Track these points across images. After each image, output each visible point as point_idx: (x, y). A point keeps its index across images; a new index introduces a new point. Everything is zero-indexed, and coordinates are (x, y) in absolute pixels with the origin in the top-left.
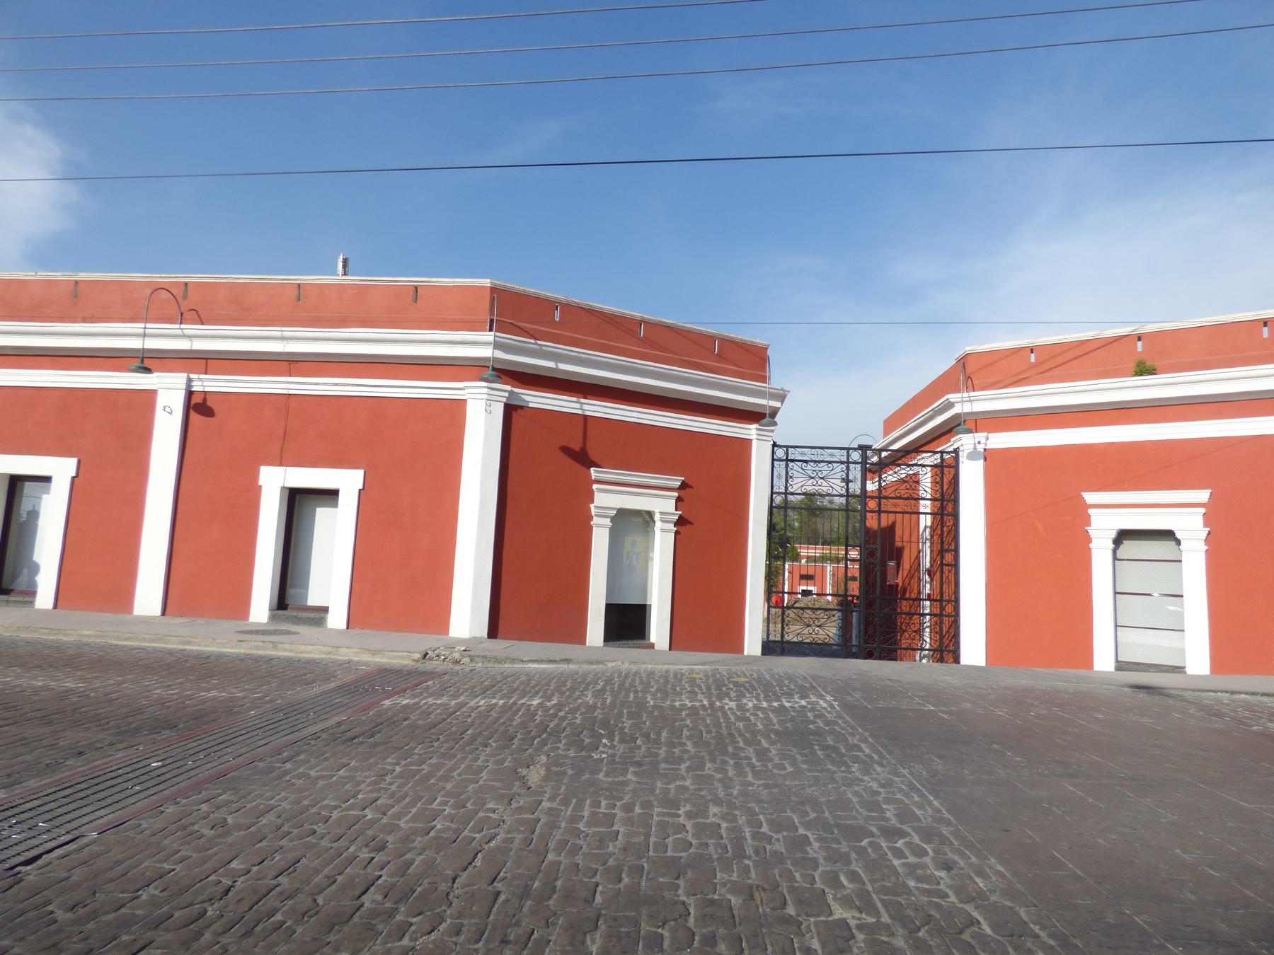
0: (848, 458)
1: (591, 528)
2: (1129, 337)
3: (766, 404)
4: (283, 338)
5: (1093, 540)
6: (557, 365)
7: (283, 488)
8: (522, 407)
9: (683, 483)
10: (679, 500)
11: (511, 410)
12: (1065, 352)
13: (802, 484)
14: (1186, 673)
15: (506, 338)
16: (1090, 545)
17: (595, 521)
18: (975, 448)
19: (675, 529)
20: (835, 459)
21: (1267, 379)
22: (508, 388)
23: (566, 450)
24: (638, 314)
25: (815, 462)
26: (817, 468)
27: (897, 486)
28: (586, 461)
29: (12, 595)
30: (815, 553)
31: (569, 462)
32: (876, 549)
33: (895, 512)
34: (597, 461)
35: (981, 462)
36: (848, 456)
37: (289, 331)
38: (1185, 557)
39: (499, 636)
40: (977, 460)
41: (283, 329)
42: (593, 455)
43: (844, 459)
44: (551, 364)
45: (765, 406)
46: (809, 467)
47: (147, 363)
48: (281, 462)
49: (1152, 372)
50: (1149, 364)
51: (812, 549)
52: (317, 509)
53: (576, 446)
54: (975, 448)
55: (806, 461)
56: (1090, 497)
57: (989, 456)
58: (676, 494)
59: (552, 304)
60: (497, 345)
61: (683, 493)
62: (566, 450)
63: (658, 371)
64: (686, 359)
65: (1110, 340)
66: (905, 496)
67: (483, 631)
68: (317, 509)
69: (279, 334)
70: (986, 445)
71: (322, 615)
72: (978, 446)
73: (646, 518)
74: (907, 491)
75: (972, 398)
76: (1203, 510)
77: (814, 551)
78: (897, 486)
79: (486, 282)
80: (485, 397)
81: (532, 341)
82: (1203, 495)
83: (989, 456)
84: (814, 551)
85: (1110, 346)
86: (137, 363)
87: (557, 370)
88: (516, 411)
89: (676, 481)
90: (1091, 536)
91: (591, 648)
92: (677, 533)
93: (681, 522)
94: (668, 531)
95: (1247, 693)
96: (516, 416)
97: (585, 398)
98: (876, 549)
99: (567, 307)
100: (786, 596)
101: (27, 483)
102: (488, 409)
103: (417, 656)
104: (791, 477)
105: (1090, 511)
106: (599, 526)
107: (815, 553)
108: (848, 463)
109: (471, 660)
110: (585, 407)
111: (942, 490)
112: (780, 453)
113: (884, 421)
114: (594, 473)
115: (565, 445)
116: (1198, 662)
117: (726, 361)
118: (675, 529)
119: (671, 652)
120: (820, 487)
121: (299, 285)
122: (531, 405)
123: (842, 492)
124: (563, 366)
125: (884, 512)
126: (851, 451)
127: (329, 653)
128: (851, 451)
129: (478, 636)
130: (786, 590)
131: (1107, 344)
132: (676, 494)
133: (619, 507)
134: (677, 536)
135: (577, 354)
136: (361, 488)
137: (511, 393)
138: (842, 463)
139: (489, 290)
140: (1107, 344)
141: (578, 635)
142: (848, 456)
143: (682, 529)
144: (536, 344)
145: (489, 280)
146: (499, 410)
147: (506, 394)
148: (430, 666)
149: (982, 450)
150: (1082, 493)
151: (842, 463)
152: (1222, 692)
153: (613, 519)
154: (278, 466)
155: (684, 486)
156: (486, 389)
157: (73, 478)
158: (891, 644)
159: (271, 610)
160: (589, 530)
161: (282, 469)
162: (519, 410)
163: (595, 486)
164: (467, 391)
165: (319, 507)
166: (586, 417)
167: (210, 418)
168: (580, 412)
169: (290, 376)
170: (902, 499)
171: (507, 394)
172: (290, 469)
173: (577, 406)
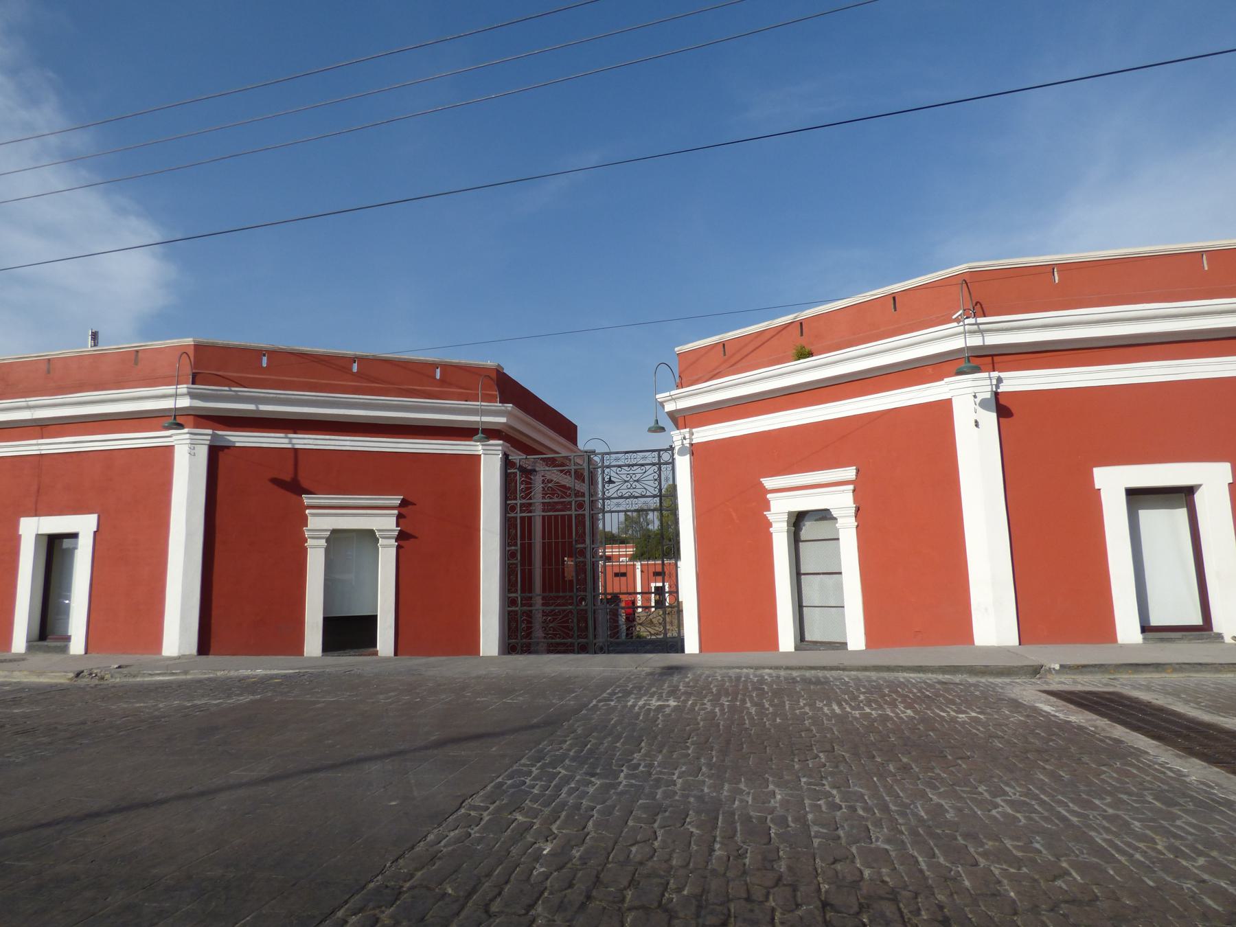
0: (659, 460)
1: (771, 535)
2: (793, 324)
3: (479, 420)
4: (29, 407)
5: (774, 525)
6: (257, 407)
7: (38, 536)
8: (228, 447)
9: (403, 501)
10: (400, 517)
11: (215, 452)
12: (746, 345)
13: (617, 488)
14: (1224, 642)
15: (200, 388)
16: (771, 529)
17: (310, 542)
18: (683, 444)
19: (397, 544)
20: (648, 462)
21: (867, 358)
22: (210, 431)
23: (276, 482)
24: (349, 352)
25: (629, 466)
26: (631, 472)
27: (619, 486)
28: (297, 488)
29: (48, 640)
30: (619, 552)
31: (281, 492)
32: (517, 550)
33: (618, 512)
34: (313, 490)
35: (688, 457)
36: (660, 457)
37: (33, 401)
38: (842, 536)
39: (212, 651)
40: (684, 455)
41: (27, 399)
42: (305, 483)
43: (656, 460)
44: (251, 407)
45: (478, 422)
46: (623, 472)
47: (179, 420)
48: (36, 513)
49: (811, 354)
50: (808, 349)
51: (622, 548)
52: (1140, 511)
53: (287, 477)
54: (683, 444)
55: (619, 466)
56: (769, 483)
57: (695, 451)
58: (396, 512)
59: (259, 353)
60: (193, 396)
61: (404, 510)
62: (276, 482)
63: (363, 402)
64: (406, 387)
65: (780, 329)
66: (626, 495)
67: (192, 648)
68: (1140, 511)
69: (24, 404)
70: (692, 440)
71: (66, 643)
72: (685, 442)
73: (369, 536)
74: (627, 490)
75: (673, 397)
76: (851, 487)
77: (611, 550)
78: (619, 486)
79: (189, 341)
80: (188, 441)
81: (227, 388)
82: (850, 473)
83: (695, 451)
84: (611, 550)
85: (780, 333)
86: (171, 420)
87: (258, 411)
88: (223, 451)
89: (396, 500)
90: (771, 521)
91: (311, 658)
92: (398, 548)
93: (402, 537)
94: (390, 546)
95: (771, 668)
96: (223, 458)
97: (295, 433)
98: (517, 550)
99: (273, 354)
100: (639, 597)
101: (65, 540)
102: (192, 452)
103: (71, 675)
104: (656, 480)
105: (769, 496)
106: (384, 546)
107: (619, 552)
108: (659, 464)
109: (112, 677)
110: (294, 441)
111: (660, 486)
112: (666, 457)
113: (576, 427)
114: (307, 499)
115: (275, 476)
116: (856, 639)
117: (450, 385)
118: (397, 544)
119: (210, 659)
120: (635, 490)
121: (49, 360)
122: (237, 445)
123: (655, 493)
124: (263, 408)
125: (608, 512)
126: (661, 453)
127: (6, 677)
128: (661, 453)
129: (187, 653)
130: (639, 590)
131: (778, 333)
132: (396, 512)
133: (331, 529)
134: (400, 550)
135: (275, 396)
136: (95, 530)
137: (214, 436)
138: (654, 464)
139: (193, 347)
140: (778, 333)
141: (296, 645)
142: (660, 457)
143: (403, 543)
144: (231, 391)
145: (191, 339)
146: (203, 453)
147: (209, 438)
148: (83, 682)
149: (688, 445)
150: (761, 480)
151: (654, 464)
152: (747, 668)
153: (328, 540)
154: (33, 516)
155: (404, 503)
156: (188, 435)
157: (95, 532)
158: (530, 639)
159: (28, 641)
160: (304, 552)
161: (37, 518)
162: (226, 450)
163: (307, 511)
164: (174, 438)
165: (1142, 509)
166: (296, 450)
167: (1010, 419)
168: (290, 446)
169: (42, 438)
170: (624, 498)
171: (209, 438)
172: (42, 518)
173: (286, 441)
